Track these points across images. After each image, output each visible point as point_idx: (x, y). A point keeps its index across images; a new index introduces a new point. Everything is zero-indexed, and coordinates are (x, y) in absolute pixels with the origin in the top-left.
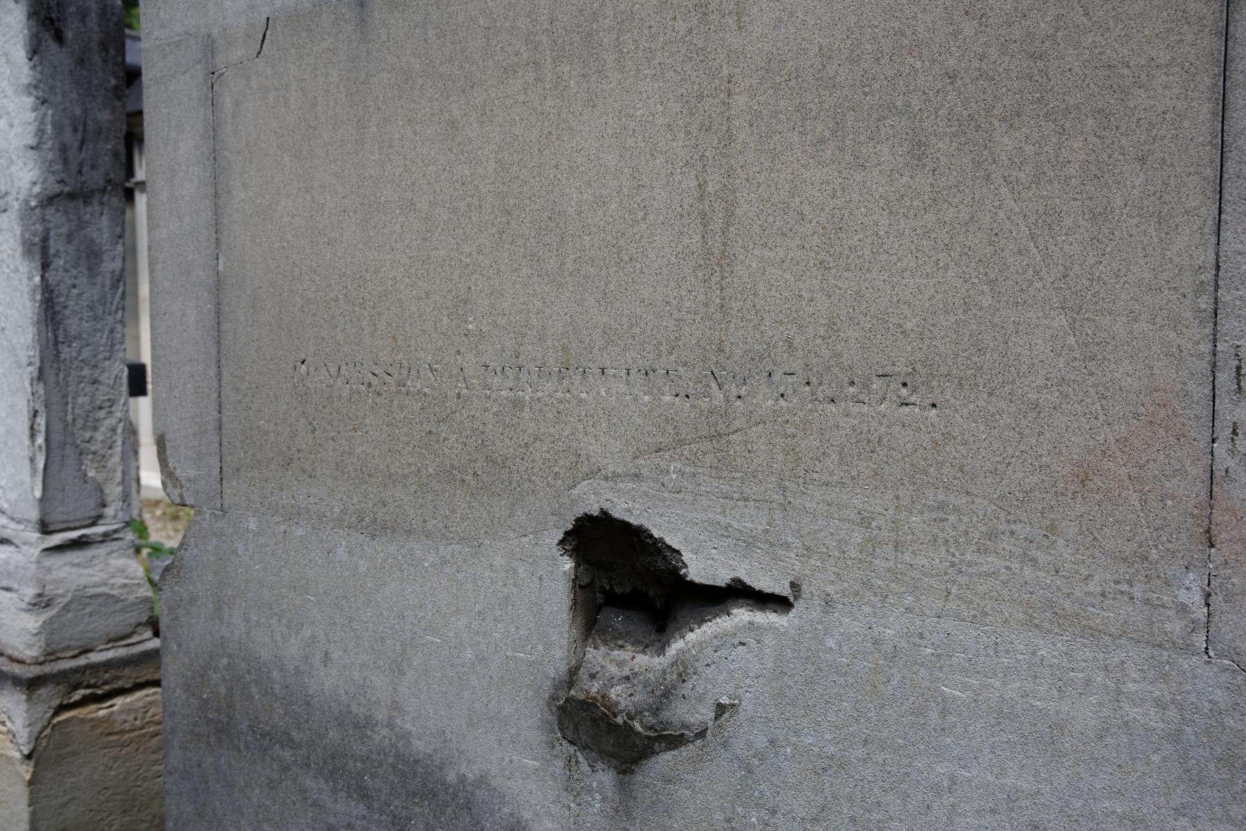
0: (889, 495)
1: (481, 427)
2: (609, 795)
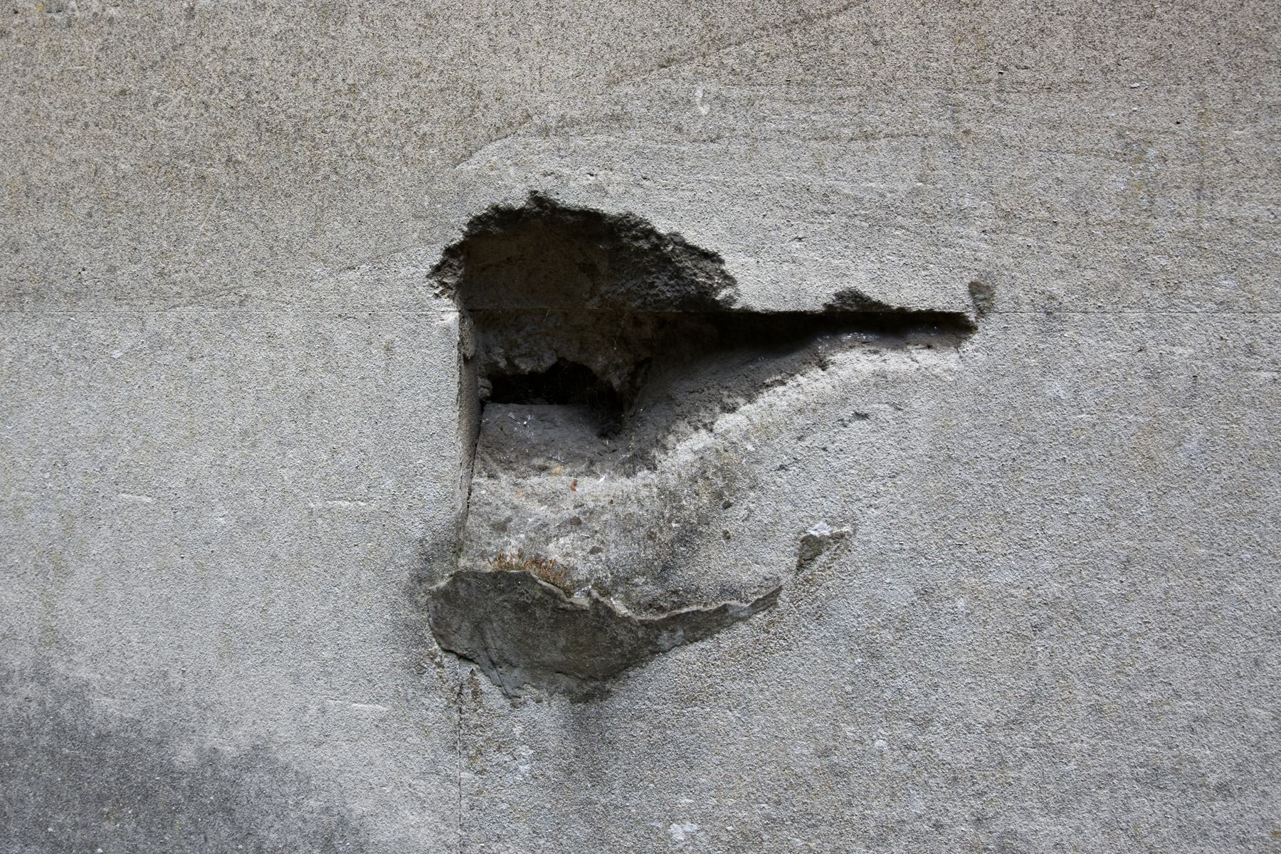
0: (1186, 93)
1: (245, 67)
2: (553, 744)
